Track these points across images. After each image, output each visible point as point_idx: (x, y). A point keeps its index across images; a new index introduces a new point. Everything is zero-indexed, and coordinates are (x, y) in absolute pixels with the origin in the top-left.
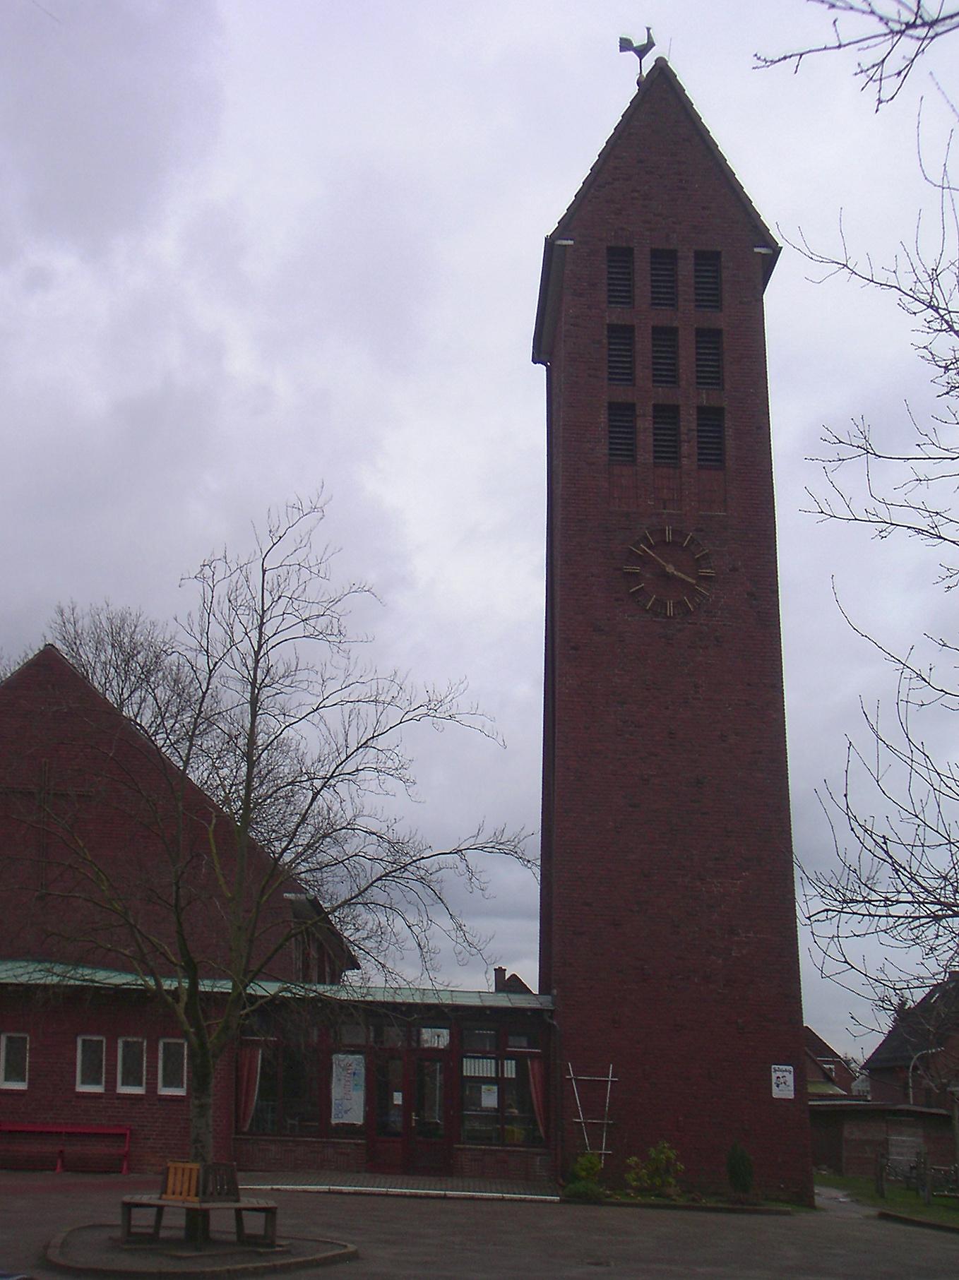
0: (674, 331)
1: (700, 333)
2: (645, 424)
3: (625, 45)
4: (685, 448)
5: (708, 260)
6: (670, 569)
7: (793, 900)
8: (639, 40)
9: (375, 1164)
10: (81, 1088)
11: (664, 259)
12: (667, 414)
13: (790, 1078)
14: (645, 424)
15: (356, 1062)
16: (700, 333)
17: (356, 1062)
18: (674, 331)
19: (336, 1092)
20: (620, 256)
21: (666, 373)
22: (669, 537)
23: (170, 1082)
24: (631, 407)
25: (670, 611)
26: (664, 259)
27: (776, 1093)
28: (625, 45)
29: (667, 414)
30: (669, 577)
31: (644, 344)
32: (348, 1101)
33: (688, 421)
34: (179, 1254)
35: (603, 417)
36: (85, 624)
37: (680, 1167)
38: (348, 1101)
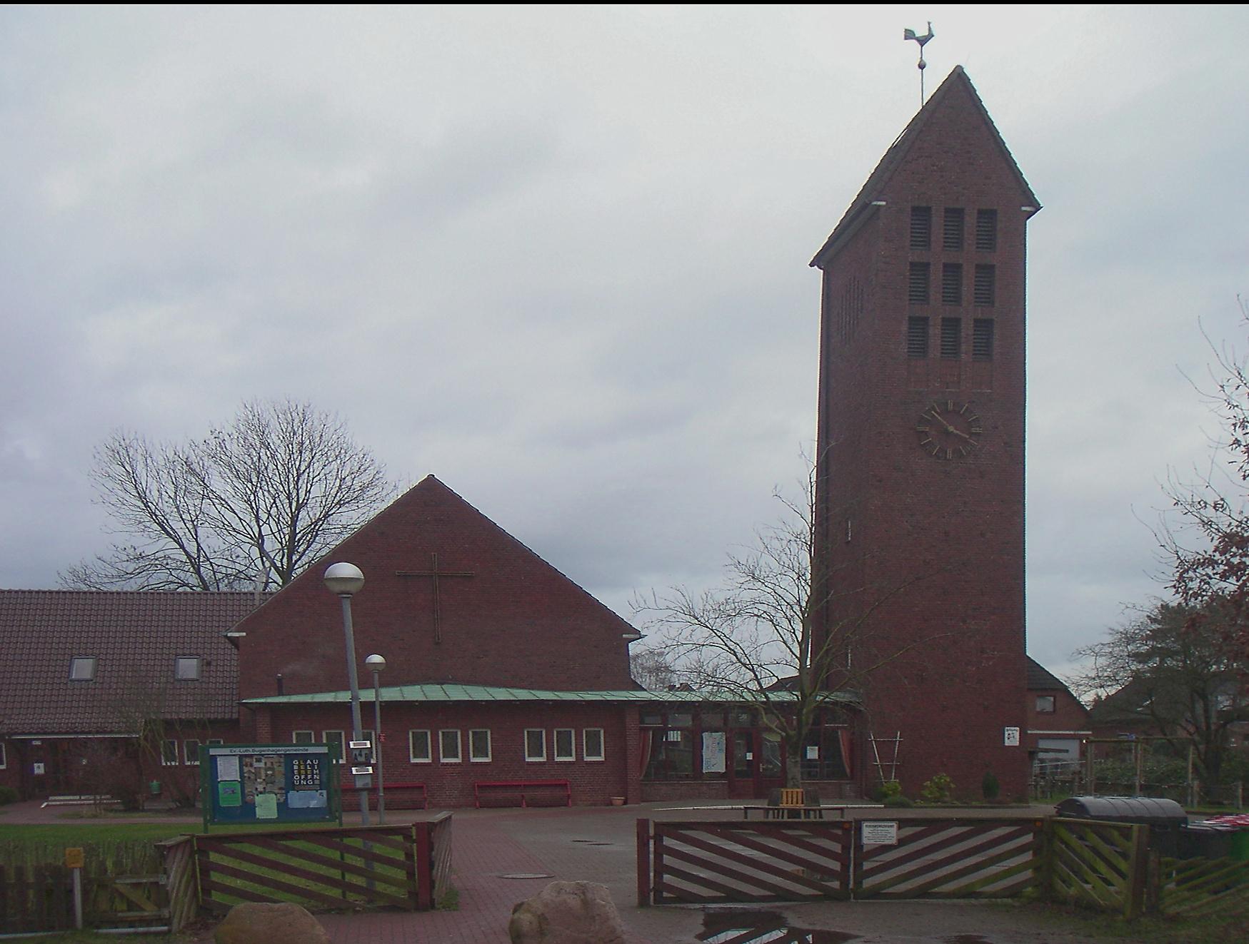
0: (959, 266)
1: (979, 267)
2: (935, 332)
3: (909, 35)
4: (964, 347)
5: (987, 215)
6: (951, 429)
7: (397, 503)
8: (921, 32)
9: (733, 793)
10: (528, 759)
11: (955, 215)
12: (952, 324)
13: (1017, 735)
14: (935, 332)
15: (720, 737)
16: (979, 267)
17: (720, 737)
18: (959, 266)
19: (706, 754)
20: (921, 213)
21: (953, 297)
22: (950, 407)
23: (480, 751)
24: (925, 320)
25: (949, 456)
26: (955, 215)
27: (1007, 743)
28: (909, 35)
29: (952, 324)
30: (948, 434)
31: (936, 275)
32: (714, 758)
33: (967, 328)
34: (814, 841)
35: (904, 328)
36: (269, 417)
37: (953, 786)
38: (714, 758)
